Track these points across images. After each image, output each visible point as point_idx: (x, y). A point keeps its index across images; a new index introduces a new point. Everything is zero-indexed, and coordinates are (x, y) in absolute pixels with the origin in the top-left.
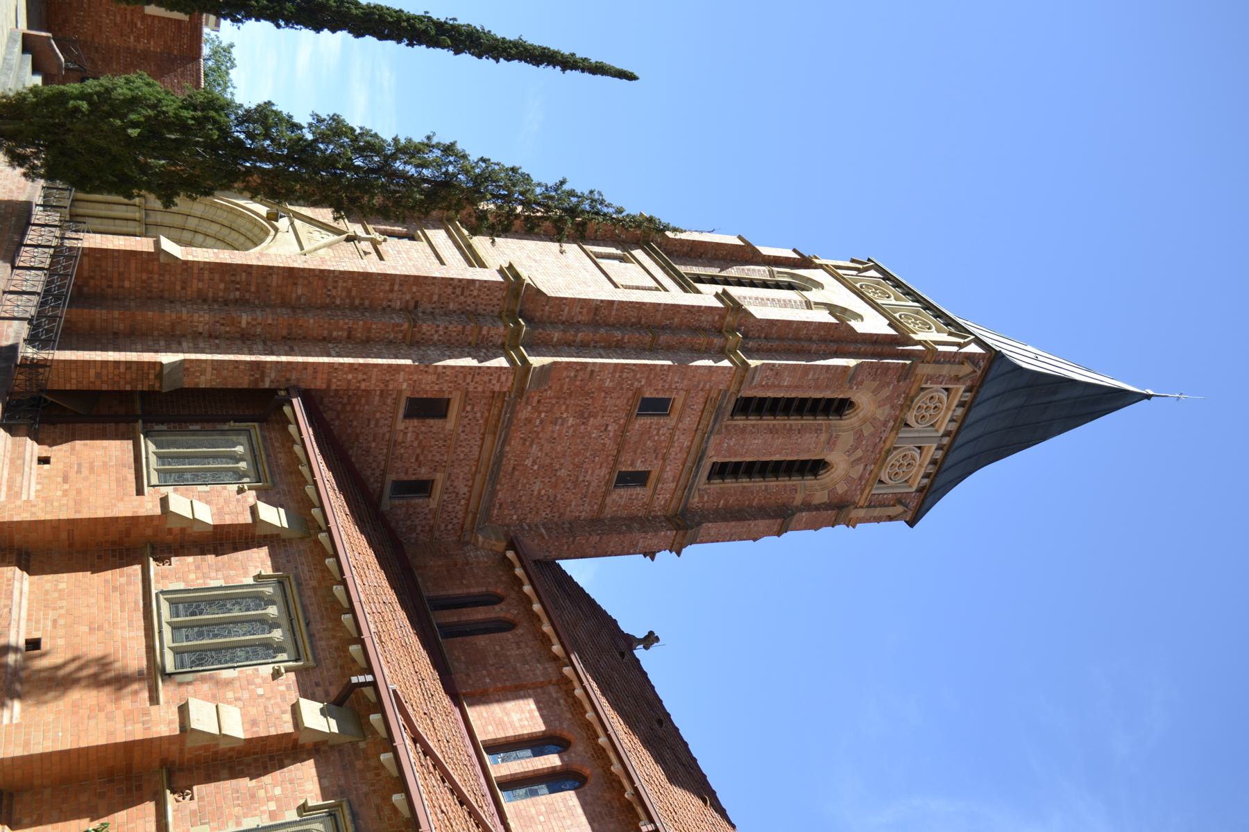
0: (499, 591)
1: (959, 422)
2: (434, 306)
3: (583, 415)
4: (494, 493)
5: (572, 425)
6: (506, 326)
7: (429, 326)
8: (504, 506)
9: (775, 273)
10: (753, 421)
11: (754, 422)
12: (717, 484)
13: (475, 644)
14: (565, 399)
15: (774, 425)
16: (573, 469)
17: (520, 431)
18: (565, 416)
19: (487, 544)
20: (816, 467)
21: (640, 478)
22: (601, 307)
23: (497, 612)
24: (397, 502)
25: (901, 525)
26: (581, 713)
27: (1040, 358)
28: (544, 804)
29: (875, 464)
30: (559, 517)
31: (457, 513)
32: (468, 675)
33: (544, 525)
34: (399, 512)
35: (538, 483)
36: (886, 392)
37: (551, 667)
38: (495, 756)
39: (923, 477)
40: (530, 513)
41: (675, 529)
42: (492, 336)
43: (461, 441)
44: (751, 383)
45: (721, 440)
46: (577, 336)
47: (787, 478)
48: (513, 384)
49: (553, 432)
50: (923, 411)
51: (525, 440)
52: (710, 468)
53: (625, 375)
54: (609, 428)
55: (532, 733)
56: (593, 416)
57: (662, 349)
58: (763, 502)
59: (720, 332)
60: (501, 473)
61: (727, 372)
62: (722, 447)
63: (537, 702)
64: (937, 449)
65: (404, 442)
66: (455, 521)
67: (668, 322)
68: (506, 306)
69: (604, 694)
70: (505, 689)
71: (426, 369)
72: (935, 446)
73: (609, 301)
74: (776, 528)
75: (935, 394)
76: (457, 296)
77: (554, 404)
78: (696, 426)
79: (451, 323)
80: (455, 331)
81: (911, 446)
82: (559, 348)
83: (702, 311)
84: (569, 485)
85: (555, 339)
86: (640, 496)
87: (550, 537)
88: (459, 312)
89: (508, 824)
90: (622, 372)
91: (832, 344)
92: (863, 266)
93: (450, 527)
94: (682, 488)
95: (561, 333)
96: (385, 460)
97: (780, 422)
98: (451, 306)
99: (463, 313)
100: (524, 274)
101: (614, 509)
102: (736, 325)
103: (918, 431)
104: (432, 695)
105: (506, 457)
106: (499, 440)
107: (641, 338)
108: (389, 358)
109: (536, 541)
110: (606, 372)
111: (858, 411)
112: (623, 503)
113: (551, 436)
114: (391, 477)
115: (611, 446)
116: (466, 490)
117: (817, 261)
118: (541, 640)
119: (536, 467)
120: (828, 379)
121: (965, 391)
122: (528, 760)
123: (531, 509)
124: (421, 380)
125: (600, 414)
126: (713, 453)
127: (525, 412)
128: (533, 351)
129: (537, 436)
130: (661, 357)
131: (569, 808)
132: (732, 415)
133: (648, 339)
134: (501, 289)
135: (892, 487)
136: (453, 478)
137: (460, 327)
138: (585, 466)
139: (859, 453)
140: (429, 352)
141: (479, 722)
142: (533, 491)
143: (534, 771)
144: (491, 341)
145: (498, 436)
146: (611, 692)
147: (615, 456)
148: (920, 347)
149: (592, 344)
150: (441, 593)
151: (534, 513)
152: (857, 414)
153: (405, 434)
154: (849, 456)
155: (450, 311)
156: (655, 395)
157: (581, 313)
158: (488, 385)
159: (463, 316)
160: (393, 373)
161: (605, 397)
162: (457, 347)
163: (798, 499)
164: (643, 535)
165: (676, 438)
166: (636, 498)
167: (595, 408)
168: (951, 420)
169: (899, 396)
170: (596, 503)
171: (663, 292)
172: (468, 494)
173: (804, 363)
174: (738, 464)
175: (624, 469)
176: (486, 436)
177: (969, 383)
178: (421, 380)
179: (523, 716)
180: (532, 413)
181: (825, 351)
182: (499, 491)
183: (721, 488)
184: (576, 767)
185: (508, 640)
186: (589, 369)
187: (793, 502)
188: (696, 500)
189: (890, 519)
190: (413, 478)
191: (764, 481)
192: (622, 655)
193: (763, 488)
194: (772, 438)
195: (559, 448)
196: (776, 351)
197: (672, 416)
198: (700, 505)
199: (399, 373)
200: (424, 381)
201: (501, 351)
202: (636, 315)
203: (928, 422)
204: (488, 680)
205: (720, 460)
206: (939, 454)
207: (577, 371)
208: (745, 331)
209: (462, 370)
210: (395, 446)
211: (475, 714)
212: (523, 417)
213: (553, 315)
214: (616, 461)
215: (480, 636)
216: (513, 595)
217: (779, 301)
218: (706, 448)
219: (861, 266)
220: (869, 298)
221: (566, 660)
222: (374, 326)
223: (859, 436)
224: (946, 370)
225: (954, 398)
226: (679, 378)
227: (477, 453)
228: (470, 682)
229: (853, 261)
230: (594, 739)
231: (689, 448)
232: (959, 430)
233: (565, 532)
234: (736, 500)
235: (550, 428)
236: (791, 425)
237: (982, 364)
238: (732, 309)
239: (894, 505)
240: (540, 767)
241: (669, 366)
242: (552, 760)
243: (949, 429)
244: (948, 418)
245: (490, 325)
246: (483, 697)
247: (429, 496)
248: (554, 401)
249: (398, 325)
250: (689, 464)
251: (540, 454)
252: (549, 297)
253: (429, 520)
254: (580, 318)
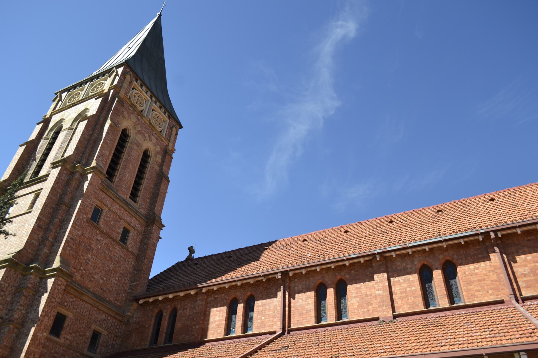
0: (157, 311)
1: (148, 90)
2: (5, 308)
3: (89, 249)
4: (109, 302)
5: (92, 256)
6: (31, 274)
7: (16, 314)
8: (117, 298)
9: (47, 137)
10: (117, 174)
11: (118, 174)
12: (139, 199)
13: (179, 328)
14: (78, 255)
15: (123, 166)
16: (111, 261)
17: (85, 281)
18: (86, 258)
19: (132, 311)
20: (146, 156)
21: (126, 232)
22: (39, 224)
23: (166, 315)
24: (98, 351)
25: (180, 131)
26: (224, 289)
27: (130, 46)
28: (258, 315)
29: (153, 131)
30: (130, 274)
31: (113, 322)
32: (193, 335)
33: (132, 282)
34: (103, 351)
35: (112, 280)
36: (126, 113)
37: (200, 297)
38: (231, 331)
39: (165, 115)
40: (124, 287)
41: (153, 224)
42: (34, 282)
43: (80, 312)
44: (102, 168)
45: (121, 191)
46: (50, 240)
47: (147, 169)
48: (64, 279)
49: (91, 266)
50: (139, 102)
51: (91, 280)
52: (131, 200)
53: (78, 224)
54: (99, 239)
55: (226, 313)
56: (91, 245)
57: (71, 202)
58: (153, 183)
59: (72, 173)
60: (102, 296)
61: (94, 177)
62: (124, 191)
63: (213, 307)
64: (156, 104)
65: (71, 341)
66: (116, 324)
67: (59, 195)
68: (20, 271)
69: (217, 277)
70: (203, 320)
71: (40, 321)
72: (154, 104)
73: (37, 219)
74: (166, 182)
75: (133, 94)
76: (5, 295)
77: (79, 261)
78: (112, 200)
79: (19, 302)
80: (24, 301)
81: (151, 113)
82: (52, 251)
83: (60, 177)
84: (118, 265)
85: (47, 251)
86: (133, 235)
87: (139, 281)
88: (13, 296)
89: (262, 333)
90: (76, 225)
91: (97, 127)
92: (58, 97)
93: (118, 327)
94: (136, 215)
95: (45, 247)
96: (76, 352)
97: (122, 162)
98: (8, 299)
99: (15, 294)
100: (6, 257)
101: (135, 248)
102: (72, 165)
103: (146, 108)
104: (202, 354)
105: (95, 291)
106: (87, 294)
107: (62, 210)
108: (27, 339)
109: (138, 288)
110: (74, 232)
111: (129, 128)
112: (134, 244)
113: (93, 267)
114: (85, 351)
115: (107, 241)
116: (104, 315)
117: (48, 116)
118: (186, 298)
119: (105, 279)
120: (112, 135)
121: (137, 82)
122: (237, 318)
123: (122, 286)
124: (45, 325)
125: (91, 241)
126: (126, 196)
127: (77, 277)
128: (49, 264)
129: (91, 274)
130: (76, 204)
131: (262, 306)
132: (112, 182)
133: (64, 207)
134: (10, 271)
135: (164, 128)
136: (96, 320)
137: (23, 298)
138: (112, 255)
139: (147, 135)
140: (31, 317)
141: (215, 335)
142: (115, 283)
143: (243, 316)
144: (36, 284)
145: (84, 293)
146: (216, 274)
147: (112, 240)
148: (112, 91)
149: (56, 234)
150: (149, 339)
151: (125, 285)
152: (130, 129)
153: (67, 339)
154: (146, 140)
155: (11, 301)
156: (91, 213)
157: (38, 235)
158: (60, 291)
159: (17, 295)
160: (36, 339)
161: (84, 236)
162: (33, 302)
163: (157, 168)
164: (151, 239)
165: (114, 210)
166: (134, 237)
167: (87, 242)
168: (146, 93)
169: (129, 109)
170: (130, 256)
171: (42, 191)
172: (106, 315)
173: (101, 142)
174: (134, 187)
175: (119, 238)
176: (82, 298)
177: (134, 79)
178: (45, 325)
179: (218, 315)
180: (79, 273)
181: (99, 131)
182: (109, 299)
183: (141, 198)
184: (246, 298)
185: (181, 313)
186: (69, 239)
187: (157, 170)
188: (143, 211)
189: (177, 134)
190: (90, 340)
191: (144, 179)
192: (196, 264)
193: (147, 180)
194: (128, 168)
195: (100, 265)
196: (91, 152)
197: (103, 209)
198: (146, 210)
199: (37, 336)
200: (46, 324)
201: (44, 280)
202: (49, 209)
203: (144, 102)
204: (198, 327)
205: (129, 194)
206: (158, 104)
207: (68, 246)
208: (76, 162)
209: (48, 302)
210: (71, 346)
211: (211, 336)
212: (79, 278)
213: (34, 249)
214: (114, 241)
215: (176, 325)
216: (160, 305)
217: (64, 141)
218: (123, 199)
219: (58, 99)
220: (77, 102)
221: (199, 289)
222: (5, 343)
223: (140, 132)
224: (125, 85)
225: (138, 88)
226: (89, 200)
227: (89, 305)
228: (196, 335)
229: (54, 101)
230: (236, 287)
231: (120, 206)
232: (151, 92)
233: (138, 274)
234: (148, 193)
235: (89, 267)
236: (125, 158)
237: (128, 70)
238: (64, 163)
239: (172, 131)
240: (242, 313)
241: (82, 202)
242: (240, 307)
243: (149, 95)
244: (145, 94)
245: (28, 282)
246: (205, 331)
247: (101, 334)
248: (77, 261)
249: (9, 331)
250: (127, 209)
251: (99, 275)
252: (24, 248)
253: (111, 337)
254: (40, 236)
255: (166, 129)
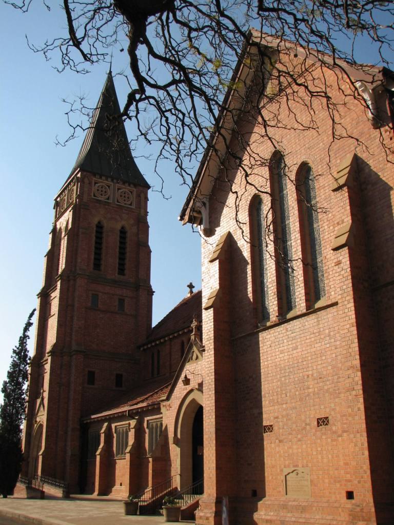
12: (126, 272)
20: (123, 232)
21: (121, 301)
148: (78, 200)
255: (135, 200)
